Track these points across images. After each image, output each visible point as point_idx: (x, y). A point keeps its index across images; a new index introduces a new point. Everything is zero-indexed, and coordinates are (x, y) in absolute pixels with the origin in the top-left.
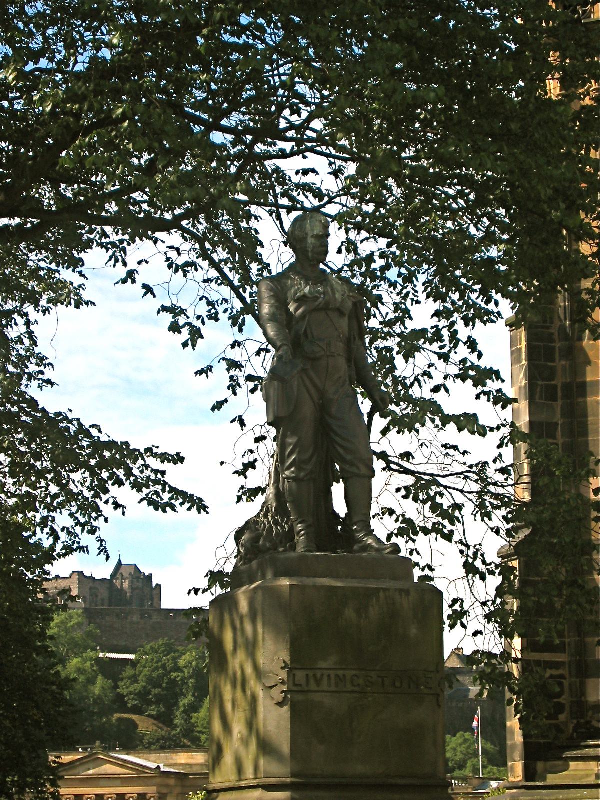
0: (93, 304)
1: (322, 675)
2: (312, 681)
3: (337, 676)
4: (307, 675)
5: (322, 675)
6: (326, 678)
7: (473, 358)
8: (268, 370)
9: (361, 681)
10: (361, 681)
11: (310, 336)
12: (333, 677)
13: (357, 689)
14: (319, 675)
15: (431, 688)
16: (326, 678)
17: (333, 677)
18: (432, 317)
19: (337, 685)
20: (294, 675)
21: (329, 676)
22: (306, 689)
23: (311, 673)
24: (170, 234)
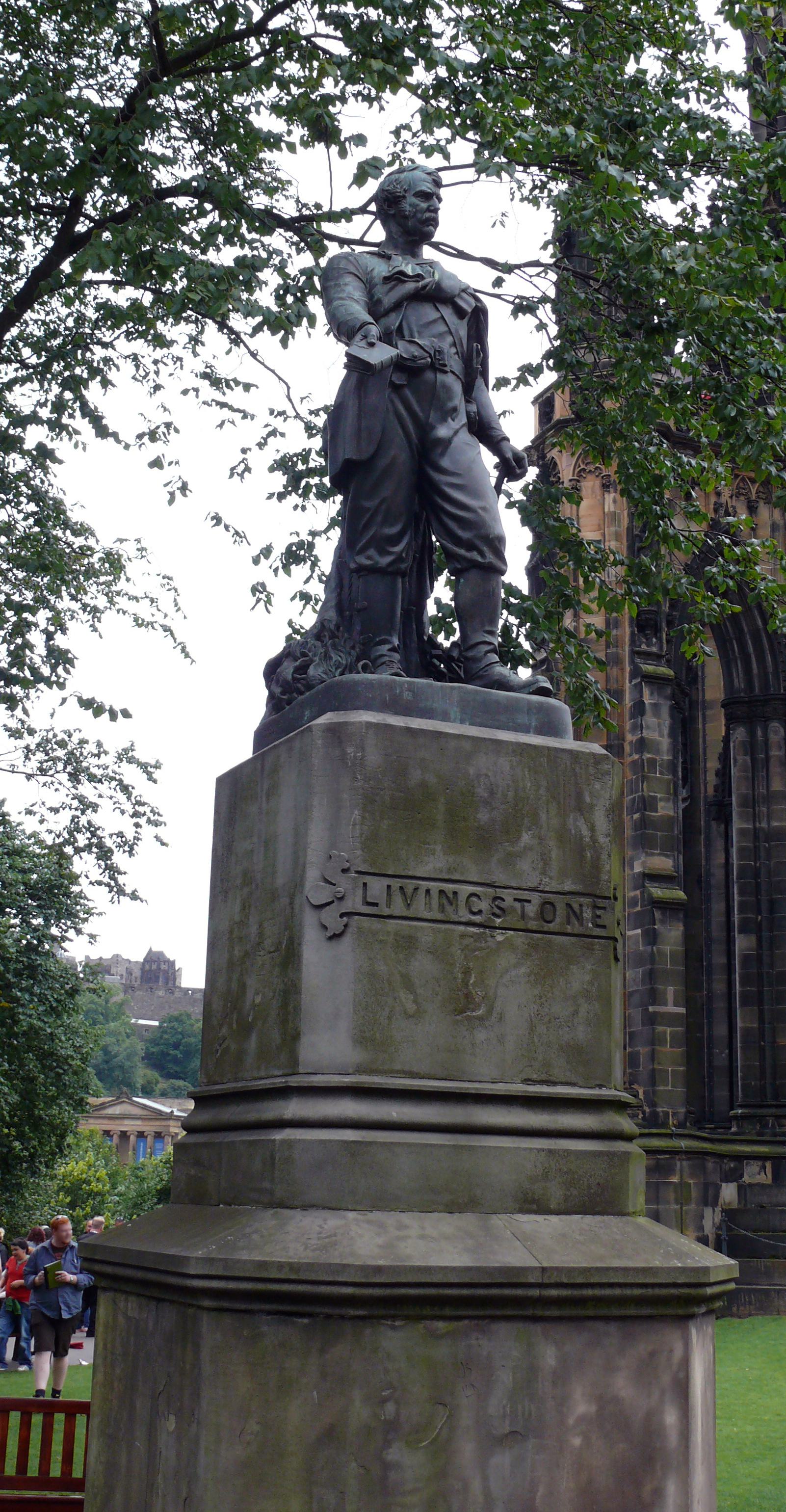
0: (126, 714)
1: (416, 889)
2: (398, 899)
3: (442, 892)
4: (389, 887)
5: (416, 889)
6: (422, 893)
7: (28, 740)
8: (747, 113)
9: (484, 905)
10: (484, 905)
11: (406, 332)
12: (435, 894)
13: (477, 919)
14: (409, 890)
15: (604, 927)
16: (422, 893)
17: (435, 894)
18: (349, 187)
19: (442, 909)
20: (365, 884)
21: (428, 891)
22: (386, 912)
23: (396, 883)
24: (293, 474)
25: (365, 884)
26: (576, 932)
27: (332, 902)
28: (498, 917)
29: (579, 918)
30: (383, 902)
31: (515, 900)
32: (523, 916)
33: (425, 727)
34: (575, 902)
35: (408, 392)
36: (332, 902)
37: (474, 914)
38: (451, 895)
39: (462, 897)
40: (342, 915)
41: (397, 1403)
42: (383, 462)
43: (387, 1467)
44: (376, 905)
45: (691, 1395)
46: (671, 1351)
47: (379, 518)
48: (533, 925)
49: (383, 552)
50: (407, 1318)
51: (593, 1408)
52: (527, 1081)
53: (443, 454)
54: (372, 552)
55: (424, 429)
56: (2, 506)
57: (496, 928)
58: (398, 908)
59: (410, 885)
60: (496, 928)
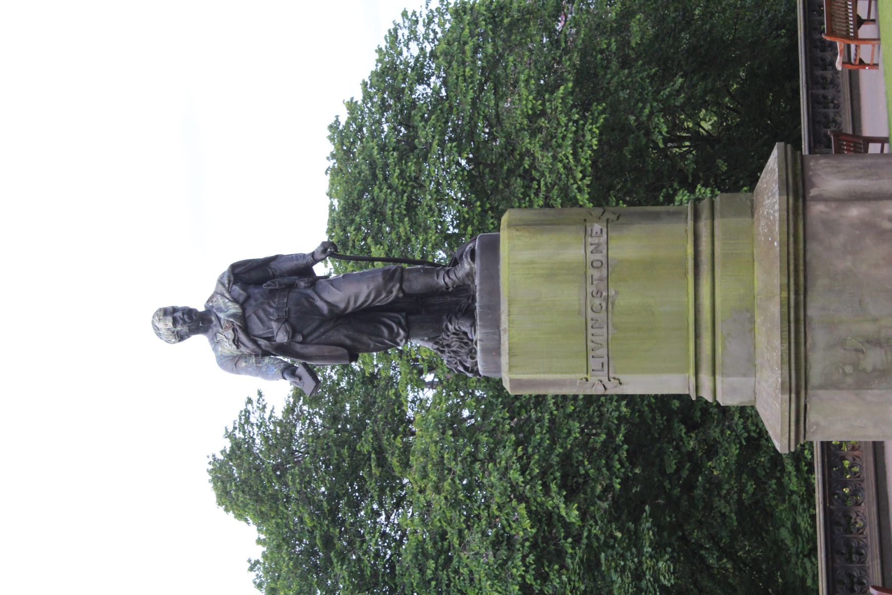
6: (594, 338)
9: (597, 301)
12: (593, 331)
13: (604, 305)
16: (594, 338)
23: (591, 354)
29: (598, 245)
30: (601, 360)
32: (600, 280)
34: (590, 248)
35: (306, 332)
39: (594, 315)
41: (845, 365)
42: (348, 342)
43: (874, 370)
46: (821, 212)
47: (380, 339)
49: (398, 334)
50: (821, 153)
51: (849, 257)
52: (686, 274)
53: (337, 307)
54: (398, 340)
55: (324, 320)
58: (603, 351)
59: (590, 345)
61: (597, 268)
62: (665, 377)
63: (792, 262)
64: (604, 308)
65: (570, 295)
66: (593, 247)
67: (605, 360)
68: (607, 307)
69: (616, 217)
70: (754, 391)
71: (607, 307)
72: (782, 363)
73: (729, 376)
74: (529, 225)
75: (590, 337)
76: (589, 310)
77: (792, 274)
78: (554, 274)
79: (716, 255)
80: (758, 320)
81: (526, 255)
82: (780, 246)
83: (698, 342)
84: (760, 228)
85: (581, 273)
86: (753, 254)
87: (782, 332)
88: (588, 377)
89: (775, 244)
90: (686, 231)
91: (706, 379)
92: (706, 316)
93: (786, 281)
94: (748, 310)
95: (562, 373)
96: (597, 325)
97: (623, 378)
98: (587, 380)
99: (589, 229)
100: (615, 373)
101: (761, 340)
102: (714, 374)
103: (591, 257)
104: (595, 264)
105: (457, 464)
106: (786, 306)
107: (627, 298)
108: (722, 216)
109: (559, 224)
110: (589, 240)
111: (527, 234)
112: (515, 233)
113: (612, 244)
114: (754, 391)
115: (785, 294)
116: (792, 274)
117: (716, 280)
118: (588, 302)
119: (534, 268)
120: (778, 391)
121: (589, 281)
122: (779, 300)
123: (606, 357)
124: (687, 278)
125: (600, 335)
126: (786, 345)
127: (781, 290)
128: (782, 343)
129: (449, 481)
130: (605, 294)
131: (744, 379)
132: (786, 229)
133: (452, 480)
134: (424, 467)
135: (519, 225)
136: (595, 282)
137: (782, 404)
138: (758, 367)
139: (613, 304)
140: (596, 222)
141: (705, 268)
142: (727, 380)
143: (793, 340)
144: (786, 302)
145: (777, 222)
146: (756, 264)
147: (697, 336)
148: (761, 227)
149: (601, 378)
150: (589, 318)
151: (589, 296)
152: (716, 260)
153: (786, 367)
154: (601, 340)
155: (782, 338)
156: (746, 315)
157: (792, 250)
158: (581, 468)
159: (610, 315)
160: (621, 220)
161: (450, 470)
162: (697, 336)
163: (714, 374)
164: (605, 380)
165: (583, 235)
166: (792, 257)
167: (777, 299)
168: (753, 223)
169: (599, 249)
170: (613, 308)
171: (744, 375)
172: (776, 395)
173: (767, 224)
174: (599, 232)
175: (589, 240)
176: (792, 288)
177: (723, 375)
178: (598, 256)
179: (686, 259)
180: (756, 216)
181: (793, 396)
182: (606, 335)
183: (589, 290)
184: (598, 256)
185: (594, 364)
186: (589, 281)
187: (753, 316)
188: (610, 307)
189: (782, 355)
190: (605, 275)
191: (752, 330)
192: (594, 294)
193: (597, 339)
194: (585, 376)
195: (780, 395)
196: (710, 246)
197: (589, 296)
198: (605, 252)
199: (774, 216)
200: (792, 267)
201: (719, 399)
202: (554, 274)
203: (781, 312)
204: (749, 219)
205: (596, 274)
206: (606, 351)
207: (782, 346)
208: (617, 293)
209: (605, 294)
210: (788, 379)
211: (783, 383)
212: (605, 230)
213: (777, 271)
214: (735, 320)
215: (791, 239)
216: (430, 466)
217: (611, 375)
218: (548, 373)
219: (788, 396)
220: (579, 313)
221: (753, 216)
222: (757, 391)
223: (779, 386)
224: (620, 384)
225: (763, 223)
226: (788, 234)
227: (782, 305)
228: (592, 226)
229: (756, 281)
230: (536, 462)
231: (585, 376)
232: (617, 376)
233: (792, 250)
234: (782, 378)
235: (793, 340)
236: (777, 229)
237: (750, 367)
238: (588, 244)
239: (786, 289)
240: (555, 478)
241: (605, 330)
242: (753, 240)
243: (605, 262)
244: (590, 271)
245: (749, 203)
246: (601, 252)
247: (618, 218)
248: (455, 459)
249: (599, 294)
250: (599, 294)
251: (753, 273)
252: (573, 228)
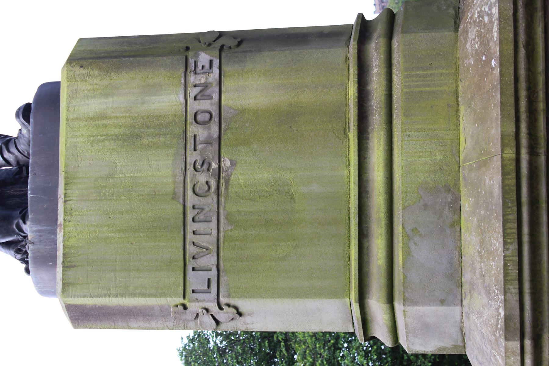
4: (194, 269)
6: (196, 239)
9: (202, 178)
16: (196, 239)
25: (193, 291)
26: (217, 89)
27: (212, 315)
28: (210, 165)
29: (206, 86)
30: (206, 275)
31: (195, 150)
32: (208, 142)
33: (59, 187)
34: (193, 92)
36: (212, 315)
37: (209, 188)
38: (196, 211)
40: (221, 308)
44: (209, 280)
45: (545, 118)
48: (215, 129)
52: (346, 131)
56: (291, 362)
57: (220, 167)
58: (210, 260)
59: (191, 250)
60: (220, 167)
61: (204, 123)
62: (311, 304)
63: (523, 94)
64: (213, 188)
65: (160, 168)
66: (196, 91)
67: (213, 275)
68: (218, 188)
69: (236, 42)
70: (461, 330)
71: (218, 188)
72: (506, 281)
73: (416, 303)
74: (98, 58)
75: (189, 236)
76: (190, 192)
77: (523, 116)
78: (136, 134)
79: (395, 97)
80: (466, 204)
81: (95, 106)
82: (501, 65)
83: (366, 245)
84: (468, 46)
85: (178, 131)
86: (457, 92)
87: (505, 222)
88: (186, 302)
89: (493, 63)
90: (347, 59)
91: (377, 306)
92: (377, 200)
93: (511, 129)
94: (448, 189)
95: (144, 295)
96: (201, 217)
97: (243, 304)
98: (185, 307)
99: (191, 62)
100: (229, 296)
101: (471, 240)
102: (390, 300)
103: (194, 106)
104: (200, 118)
105: (325, 351)
106: (514, 175)
107: (248, 171)
108: (404, 32)
109: (144, 56)
110: (192, 78)
111: (96, 72)
112: (79, 71)
113: (227, 84)
114: (461, 330)
115: (510, 153)
116: (523, 116)
117: (395, 140)
118: (188, 180)
119: (106, 126)
120: (500, 334)
121: (190, 145)
122: (499, 163)
123: (214, 269)
124: (347, 137)
125: (205, 233)
126: (513, 247)
127: (503, 146)
128: (505, 243)
129: (320, 362)
130: (214, 166)
131: (442, 309)
132: (512, 35)
133: (322, 361)
134: (305, 352)
135: (85, 59)
136: (199, 147)
137: (507, 357)
138: (466, 287)
139: (227, 182)
140: (203, 50)
141: (377, 120)
142: (413, 310)
143: (526, 238)
144: (513, 167)
145: (496, 23)
146: (462, 108)
147: (363, 234)
148: (471, 41)
149: (207, 305)
150: (189, 205)
151: (190, 169)
152: (395, 106)
153: (514, 289)
154: (208, 241)
155: (505, 235)
156: (445, 198)
157: (522, 72)
158: (405, 355)
159: (222, 199)
160: (243, 46)
161: (321, 354)
162: (363, 234)
163: (390, 300)
164: (213, 307)
165: (182, 70)
166: (523, 85)
167: (497, 163)
168: (457, 39)
169: (208, 92)
170: (227, 188)
171: (442, 302)
172: (497, 340)
173: (479, 34)
174: (207, 66)
175: (192, 78)
176: (524, 141)
177: (405, 301)
178: (205, 105)
179: (347, 105)
180: (461, 27)
181: (528, 343)
182: (215, 232)
183: (190, 161)
184: (205, 105)
185: (196, 280)
186: (190, 145)
187: (457, 199)
188: (223, 187)
189: (505, 265)
190: (216, 135)
191: (456, 224)
192: (198, 166)
193: (201, 240)
194: (181, 300)
195: (502, 341)
196: (384, 82)
197: (190, 169)
198: (216, 97)
199: (490, 15)
200: (523, 103)
201: (403, 342)
202: (136, 134)
203: (504, 186)
204: (449, 34)
205: (201, 133)
206: (215, 258)
207: (505, 249)
208: (233, 163)
209: (214, 166)
210: (517, 312)
211: (507, 319)
212: (216, 62)
213: (496, 112)
214: (426, 206)
215: (522, 53)
216: (308, 352)
217: (223, 300)
218: (123, 295)
219: (517, 344)
220: (174, 196)
221: (456, 29)
222: (466, 330)
223: (501, 324)
224: (240, 314)
225: (472, 35)
226: (516, 21)
227: (504, 174)
228: (197, 56)
229: (462, 139)
230: (375, 351)
231: (181, 300)
232: (233, 302)
233: (522, 72)
234: (505, 309)
235: (526, 238)
236: (495, 35)
237: (452, 288)
238: (190, 84)
239: (513, 143)
240: (388, 362)
241: (214, 224)
242: (457, 69)
243: (215, 113)
244: (193, 129)
245: (452, 11)
246: (211, 98)
247: (239, 44)
248: (324, 348)
249: (205, 167)
250: (205, 167)
251: (458, 125)
252: (167, 60)
